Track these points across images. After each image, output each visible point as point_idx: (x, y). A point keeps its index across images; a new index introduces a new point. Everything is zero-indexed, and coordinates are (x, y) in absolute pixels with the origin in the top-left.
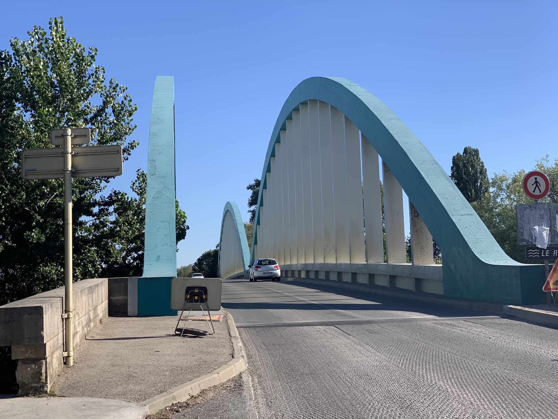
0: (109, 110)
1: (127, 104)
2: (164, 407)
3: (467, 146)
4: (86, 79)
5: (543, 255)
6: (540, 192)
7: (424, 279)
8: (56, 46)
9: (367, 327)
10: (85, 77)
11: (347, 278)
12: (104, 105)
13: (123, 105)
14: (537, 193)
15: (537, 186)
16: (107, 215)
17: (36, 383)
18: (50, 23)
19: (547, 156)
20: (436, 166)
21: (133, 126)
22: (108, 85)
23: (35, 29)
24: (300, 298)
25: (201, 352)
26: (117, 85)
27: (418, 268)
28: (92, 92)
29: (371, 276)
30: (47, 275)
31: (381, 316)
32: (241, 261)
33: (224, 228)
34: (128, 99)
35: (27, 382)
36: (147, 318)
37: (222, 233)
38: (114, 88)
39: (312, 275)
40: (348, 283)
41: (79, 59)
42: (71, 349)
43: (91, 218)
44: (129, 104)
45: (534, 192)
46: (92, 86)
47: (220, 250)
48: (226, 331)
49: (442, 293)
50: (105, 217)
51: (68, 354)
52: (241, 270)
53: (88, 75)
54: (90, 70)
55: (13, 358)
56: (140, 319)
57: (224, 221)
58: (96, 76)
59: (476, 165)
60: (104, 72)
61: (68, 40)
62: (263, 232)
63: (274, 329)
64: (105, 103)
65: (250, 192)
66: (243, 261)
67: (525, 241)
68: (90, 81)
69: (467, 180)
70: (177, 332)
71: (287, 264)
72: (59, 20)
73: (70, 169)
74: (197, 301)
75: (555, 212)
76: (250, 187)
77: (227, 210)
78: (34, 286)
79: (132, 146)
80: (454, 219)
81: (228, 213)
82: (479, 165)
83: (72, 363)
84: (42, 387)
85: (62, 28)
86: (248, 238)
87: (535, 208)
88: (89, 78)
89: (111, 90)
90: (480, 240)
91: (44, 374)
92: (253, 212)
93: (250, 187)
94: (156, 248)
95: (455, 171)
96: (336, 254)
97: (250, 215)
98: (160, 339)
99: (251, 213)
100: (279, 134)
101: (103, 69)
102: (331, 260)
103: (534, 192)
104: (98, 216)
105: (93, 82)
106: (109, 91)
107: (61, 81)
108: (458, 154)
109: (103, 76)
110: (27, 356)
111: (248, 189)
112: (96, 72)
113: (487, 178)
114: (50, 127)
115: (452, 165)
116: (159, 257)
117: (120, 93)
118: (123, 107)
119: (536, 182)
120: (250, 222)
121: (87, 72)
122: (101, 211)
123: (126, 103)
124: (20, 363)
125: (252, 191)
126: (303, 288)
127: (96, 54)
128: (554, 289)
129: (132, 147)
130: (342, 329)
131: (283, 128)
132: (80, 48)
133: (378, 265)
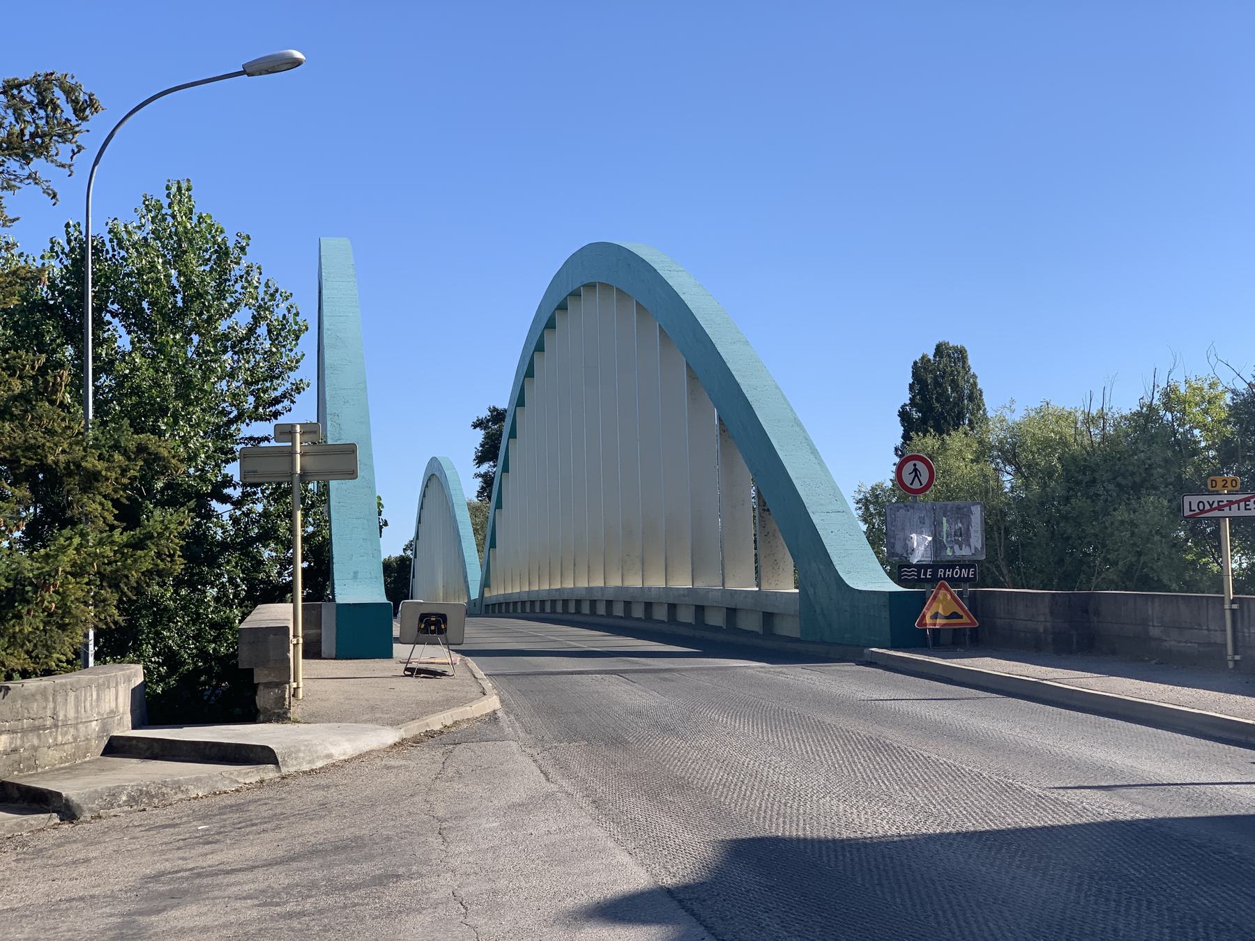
0: (262, 330)
1: (291, 320)
2: (418, 733)
3: (941, 340)
4: (231, 283)
5: (922, 577)
6: (921, 484)
7: (777, 614)
8: (181, 229)
9: (662, 675)
10: (229, 281)
11: (660, 614)
12: (256, 323)
13: (285, 322)
14: (916, 486)
15: (916, 475)
16: (254, 503)
17: (279, 709)
18: (168, 188)
19: (1013, 401)
20: (798, 429)
21: (299, 354)
22: (262, 289)
23: (144, 201)
24: (574, 644)
25: (446, 690)
26: (277, 291)
27: (767, 594)
28: (239, 304)
29: (700, 610)
30: (158, 601)
31: (691, 664)
32: (462, 579)
33: (425, 511)
34: (294, 311)
35: (269, 708)
36: (355, 661)
37: (419, 522)
38: (272, 295)
39: (601, 610)
40: (663, 622)
41: (223, 253)
42: (300, 680)
43: (229, 506)
44: (295, 319)
45: (911, 484)
46: (240, 294)
47: (415, 557)
48: (469, 674)
49: (799, 636)
50: (251, 505)
51: (298, 684)
52: (461, 599)
53: (233, 278)
54: (237, 271)
55: (256, 682)
56: (336, 661)
57: (424, 496)
58: (246, 278)
59: (961, 383)
60: (260, 273)
61: (200, 217)
62: (508, 525)
63: (530, 677)
64: (256, 319)
65: (480, 434)
66: (466, 582)
67: (897, 555)
68: (238, 287)
69: (942, 413)
70: (406, 673)
71: (593, 584)
72: (184, 185)
73: (299, 472)
74: (433, 632)
75: (941, 514)
76: (479, 424)
77: (433, 475)
78: (139, 618)
79: (297, 389)
80: (815, 519)
81: (434, 481)
82: (968, 382)
83: (301, 697)
84: (285, 713)
85: (190, 197)
86: (476, 531)
87: (913, 508)
88: (236, 282)
89: (267, 298)
90: (849, 552)
91: (288, 700)
92: (488, 481)
93: (479, 424)
94: (351, 559)
95: (918, 394)
96: (643, 571)
97: (478, 483)
98: (388, 679)
99: (480, 479)
100: (542, 336)
101: (258, 268)
102: (635, 582)
103: (911, 484)
104: (238, 504)
105: (242, 288)
106: (263, 299)
107: (188, 284)
108: (923, 358)
109: (259, 279)
110: (270, 679)
111: (475, 428)
112: (248, 273)
113: (983, 408)
114: (179, 364)
115: (911, 381)
116: (356, 573)
117: (280, 302)
118: (284, 325)
119: (915, 470)
120: (478, 497)
121: (232, 273)
122: (245, 495)
123: (291, 318)
124: (261, 687)
125: (483, 432)
126: (654, 643)
127: (248, 245)
128: (931, 624)
129: (298, 390)
130: (630, 678)
131: (551, 325)
132: (223, 236)
133: (708, 591)
